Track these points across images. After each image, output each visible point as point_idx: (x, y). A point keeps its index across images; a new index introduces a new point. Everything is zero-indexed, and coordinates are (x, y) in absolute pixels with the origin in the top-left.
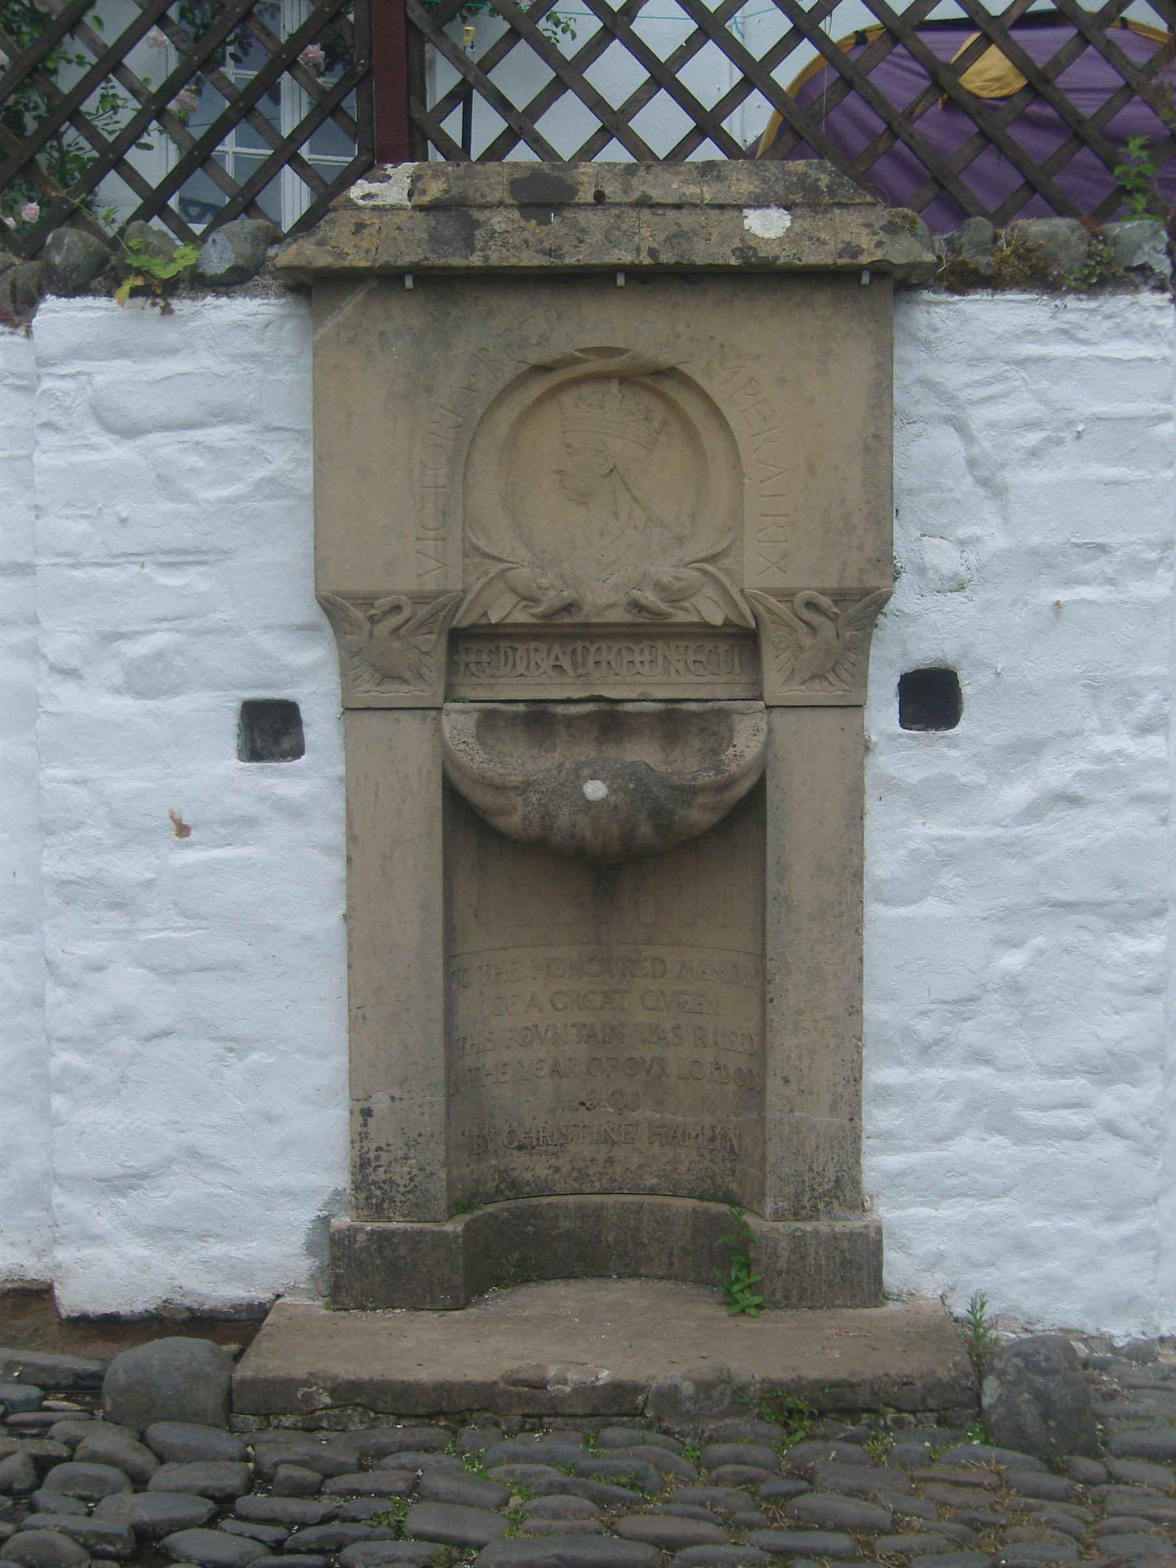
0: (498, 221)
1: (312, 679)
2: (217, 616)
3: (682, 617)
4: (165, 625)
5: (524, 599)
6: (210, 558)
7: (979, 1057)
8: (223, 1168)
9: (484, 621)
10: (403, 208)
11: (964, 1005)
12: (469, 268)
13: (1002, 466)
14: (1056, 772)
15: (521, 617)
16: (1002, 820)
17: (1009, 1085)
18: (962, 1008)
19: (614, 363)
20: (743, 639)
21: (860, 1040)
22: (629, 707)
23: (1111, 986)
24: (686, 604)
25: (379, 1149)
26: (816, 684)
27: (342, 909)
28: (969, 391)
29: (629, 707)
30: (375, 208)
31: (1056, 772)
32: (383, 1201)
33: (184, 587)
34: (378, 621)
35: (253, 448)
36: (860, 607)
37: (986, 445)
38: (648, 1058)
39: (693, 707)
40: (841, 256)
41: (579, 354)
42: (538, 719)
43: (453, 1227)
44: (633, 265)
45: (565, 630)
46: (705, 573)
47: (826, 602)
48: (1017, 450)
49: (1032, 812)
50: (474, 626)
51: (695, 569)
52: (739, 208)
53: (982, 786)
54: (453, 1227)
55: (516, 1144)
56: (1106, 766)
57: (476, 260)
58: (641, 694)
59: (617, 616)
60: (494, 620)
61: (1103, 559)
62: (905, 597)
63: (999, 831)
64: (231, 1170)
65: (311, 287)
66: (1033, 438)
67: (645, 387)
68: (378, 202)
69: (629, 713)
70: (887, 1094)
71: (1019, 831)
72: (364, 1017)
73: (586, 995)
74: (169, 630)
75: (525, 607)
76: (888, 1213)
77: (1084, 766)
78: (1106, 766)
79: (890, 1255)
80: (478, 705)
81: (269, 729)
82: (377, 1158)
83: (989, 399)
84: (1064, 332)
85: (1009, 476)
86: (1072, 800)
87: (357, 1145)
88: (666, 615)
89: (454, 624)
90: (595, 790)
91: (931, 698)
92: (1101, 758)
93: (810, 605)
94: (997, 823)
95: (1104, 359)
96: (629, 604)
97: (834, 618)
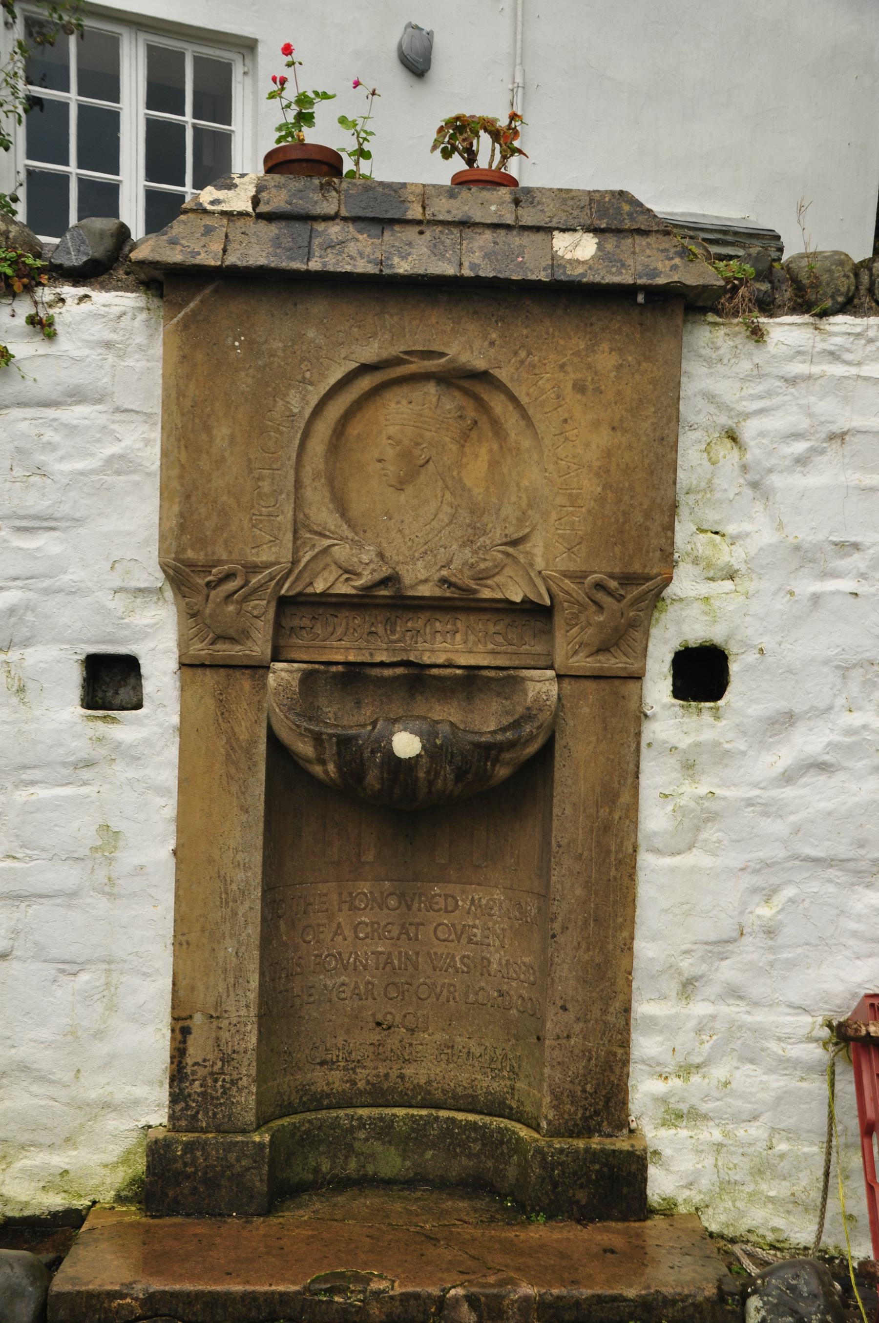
0: (335, 230)
1: (157, 641)
2: (66, 578)
3: (486, 594)
4: (19, 583)
5: (346, 571)
6: (64, 524)
7: (734, 993)
8: (50, 1082)
9: (310, 590)
10: (247, 214)
11: (720, 948)
12: (308, 272)
13: (770, 471)
14: (809, 741)
15: (343, 589)
16: (760, 782)
17: (760, 1017)
18: (720, 949)
19: (431, 365)
20: (536, 614)
21: (630, 973)
22: (435, 671)
23: (854, 934)
24: (489, 582)
25: (196, 1064)
26: (600, 657)
27: (172, 844)
28: (744, 403)
29: (435, 671)
30: (223, 213)
31: (809, 741)
32: (197, 1113)
33: (37, 549)
34: (214, 588)
35: (105, 427)
36: (636, 586)
37: (757, 451)
38: (440, 984)
39: (491, 674)
40: (640, 277)
41: (401, 355)
42: (353, 677)
43: (262, 1137)
44: (455, 277)
45: (385, 600)
46: (508, 555)
47: (613, 584)
48: (784, 457)
49: (788, 778)
50: (300, 594)
51: (499, 551)
52: (547, 230)
53: (744, 753)
54: (262, 1137)
55: (318, 1060)
56: (854, 739)
57: (315, 265)
58: (447, 660)
59: (425, 591)
60: (320, 586)
61: (857, 556)
62: (685, 583)
63: (757, 792)
64: (58, 1083)
65: (165, 283)
66: (800, 447)
67: (466, 392)
68: (225, 207)
69: (434, 677)
70: (652, 1023)
71: (775, 793)
72: (188, 943)
73: (385, 926)
74: (22, 588)
75: (347, 580)
76: (653, 1133)
77: (836, 738)
78: (854, 739)
79: (653, 1171)
80: (304, 666)
81: (109, 680)
82: (194, 1073)
83: (762, 411)
84: (832, 353)
85: (776, 480)
86: (822, 767)
87: (176, 1060)
88: (475, 591)
89: (283, 592)
90: (406, 744)
91: (702, 674)
92: (850, 731)
93: (599, 586)
94: (756, 786)
95: (867, 379)
96: (439, 581)
97: (620, 598)
